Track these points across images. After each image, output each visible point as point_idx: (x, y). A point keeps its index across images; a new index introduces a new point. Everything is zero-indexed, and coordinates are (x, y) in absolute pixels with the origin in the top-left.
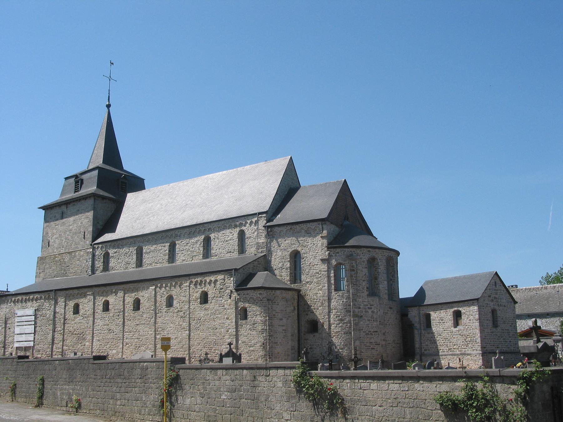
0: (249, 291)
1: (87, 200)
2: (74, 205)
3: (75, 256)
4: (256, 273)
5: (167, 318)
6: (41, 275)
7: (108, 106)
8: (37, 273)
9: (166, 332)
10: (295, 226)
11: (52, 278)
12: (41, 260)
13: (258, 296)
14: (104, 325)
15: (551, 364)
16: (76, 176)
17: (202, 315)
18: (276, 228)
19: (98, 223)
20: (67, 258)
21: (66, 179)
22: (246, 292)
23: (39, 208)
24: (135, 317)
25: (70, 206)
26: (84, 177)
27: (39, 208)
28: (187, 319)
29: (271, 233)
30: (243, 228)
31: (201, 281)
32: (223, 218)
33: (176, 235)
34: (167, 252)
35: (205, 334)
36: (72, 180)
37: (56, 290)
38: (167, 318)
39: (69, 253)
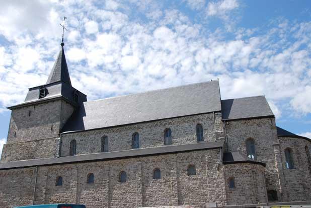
0: (236, 165)
1: (55, 103)
2: (42, 106)
3: (42, 143)
4: (277, 127)
5: (154, 187)
6: (7, 158)
7: (62, 45)
8: (2, 157)
9: (153, 199)
10: (248, 121)
11: (18, 160)
12: (6, 147)
13: (245, 168)
14: (88, 194)
15: (217, 31)
16: (41, 87)
17: (190, 184)
18: (233, 122)
19: (63, 119)
20: (34, 145)
21: (30, 89)
22: (233, 165)
23: (7, 108)
24: (121, 187)
25: (37, 107)
26: (48, 88)
27: (7, 108)
28: (175, 188)
29: (228, 126)
30: (200, 122)
31: (188, 157)
32: (121, 124)
33: (139, 128)
34: (131, 140)
35: (194, 200)
36: (38, 91)
37: (38, 166)
38: (154, 187)
39: (36, 141)
